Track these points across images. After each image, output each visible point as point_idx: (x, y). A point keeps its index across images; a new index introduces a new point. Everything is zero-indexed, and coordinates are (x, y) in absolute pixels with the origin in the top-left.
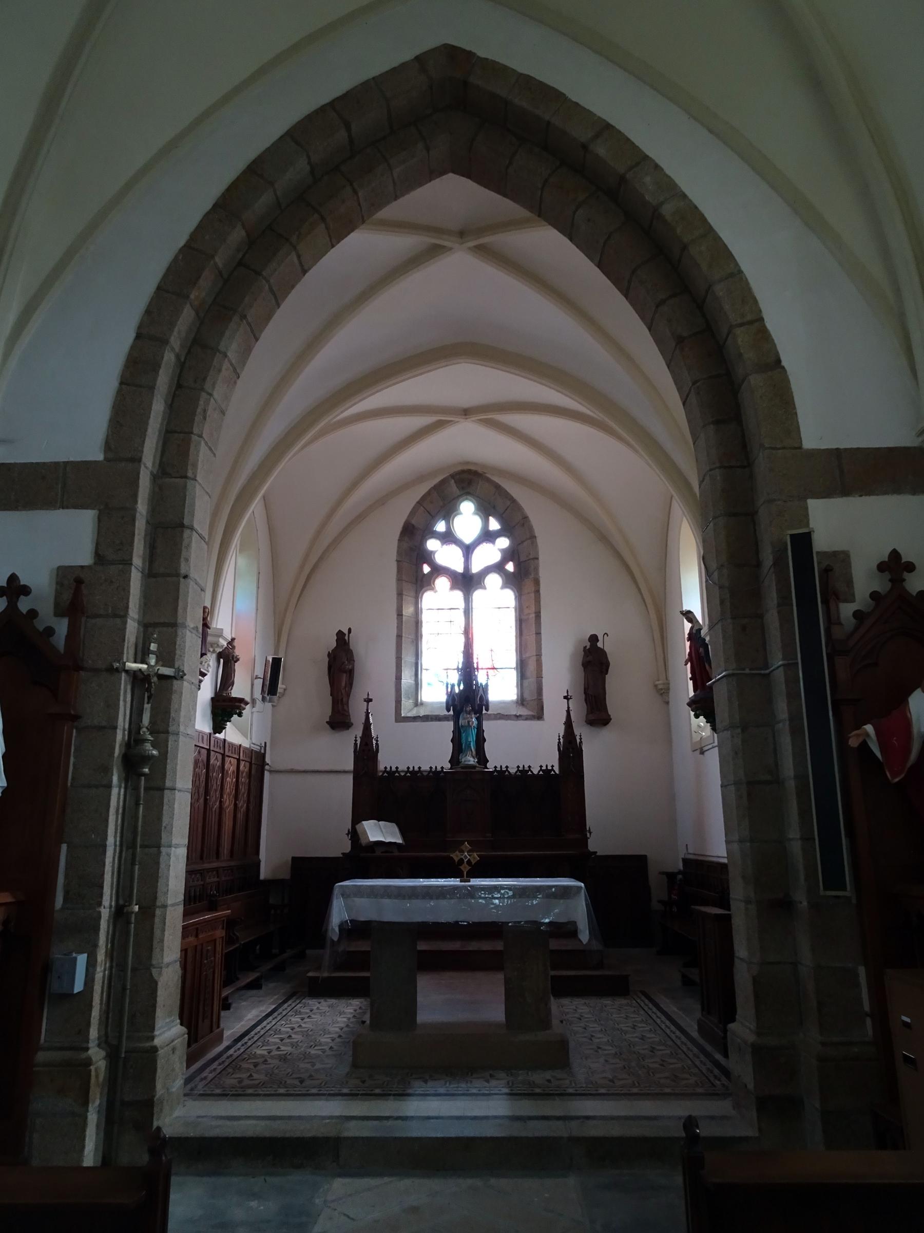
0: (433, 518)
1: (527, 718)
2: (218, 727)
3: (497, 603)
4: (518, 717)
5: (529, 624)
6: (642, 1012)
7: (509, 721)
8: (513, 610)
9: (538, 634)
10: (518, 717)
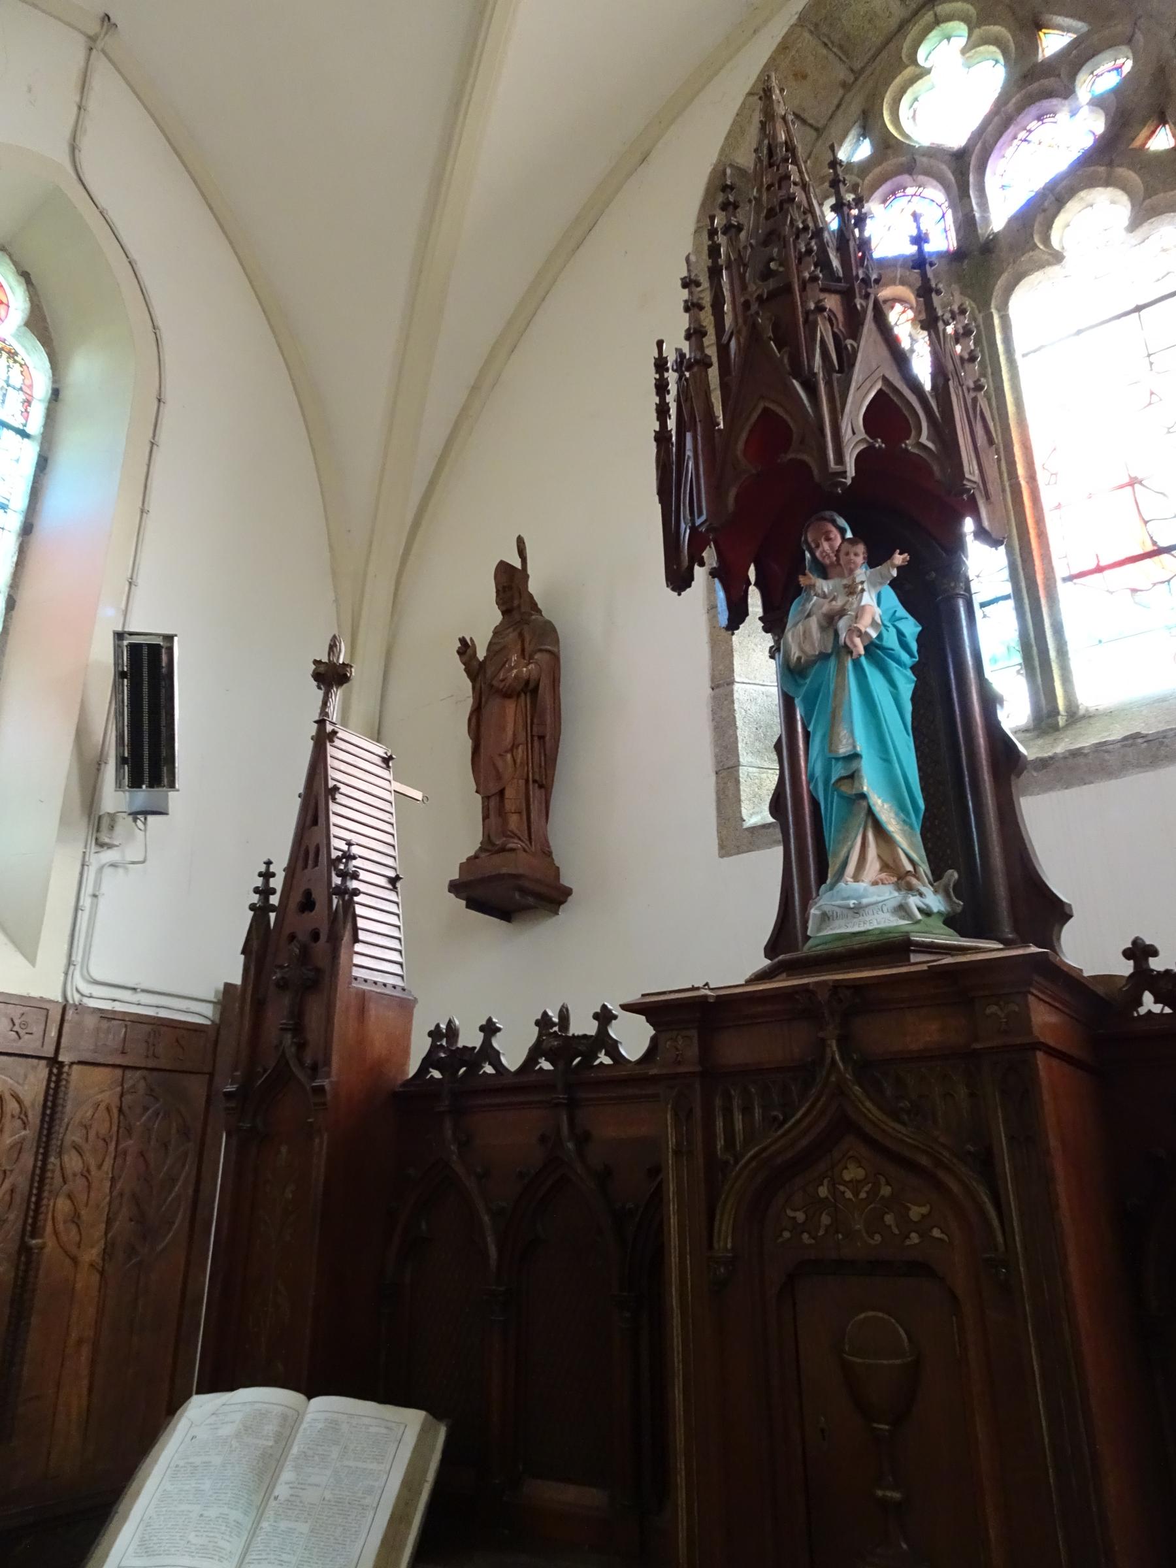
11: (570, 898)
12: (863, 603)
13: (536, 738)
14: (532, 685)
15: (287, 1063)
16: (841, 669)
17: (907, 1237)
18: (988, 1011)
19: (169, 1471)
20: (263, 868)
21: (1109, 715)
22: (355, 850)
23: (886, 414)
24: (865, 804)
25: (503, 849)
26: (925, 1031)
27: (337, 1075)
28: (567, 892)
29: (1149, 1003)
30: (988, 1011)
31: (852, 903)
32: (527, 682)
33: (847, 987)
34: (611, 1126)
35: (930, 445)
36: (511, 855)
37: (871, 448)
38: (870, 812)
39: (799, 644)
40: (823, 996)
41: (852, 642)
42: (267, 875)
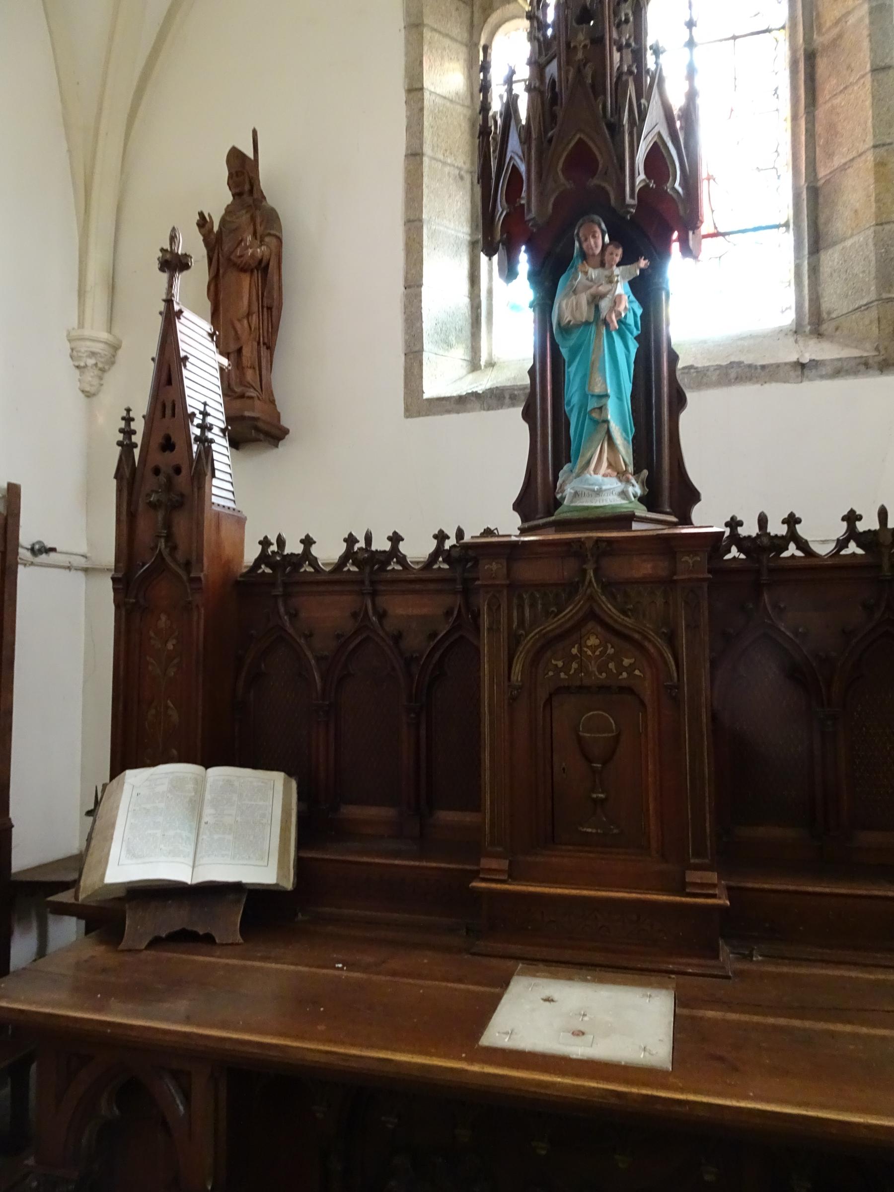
1: (839, 370)
4: (803, 369)
8: (783, 36)
10: (803, 369)
11: (287, 437)
12: (617, 292)
13: (265, 309)
14: (263, 265)
15: (163, 559)
16: (598, 334)
17: (621, 674)
18: (683, 560)
19: (130, 814)
20: (124, 414)
22: (209, 410)
24: (606, 426)
25: (242, 396)
26: (644, 568)
27: (208, 570)
28: (286, 432)
29: (734, 552)
30: (683, 560)
31: (596, 488)
32: (261, 261)
33: (604, 541)
34: (402, 609)
35: (680, 190)
36: (249, 402)
37: (647, 186)
38: (608, 432)
39: (572, 311)
40: (589, 545)
41: (611, 318)
42: (128, 420)
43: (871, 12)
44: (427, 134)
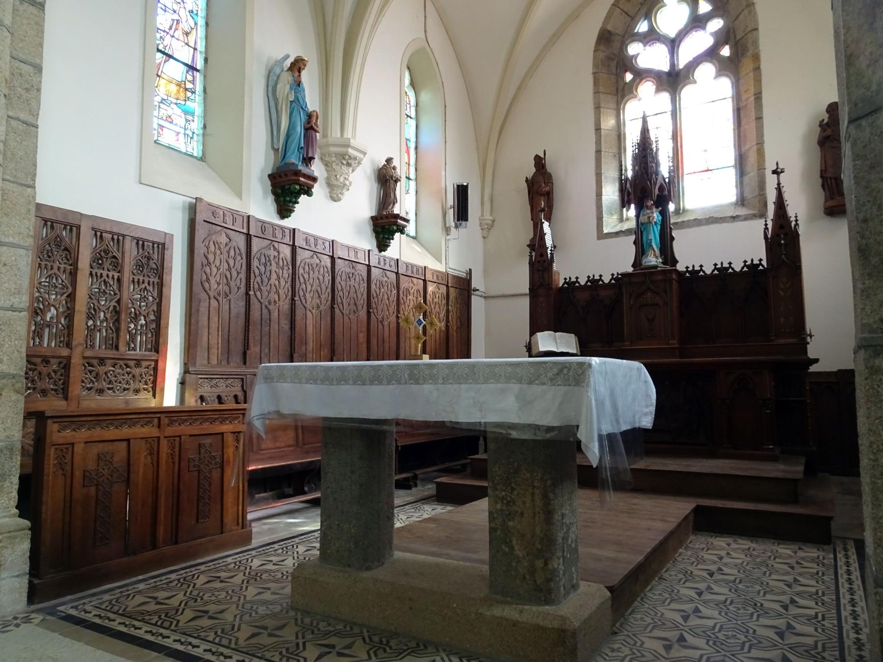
0: (633, 20)
1: (746, 218)
2: (382, 245)
3: (711, 96)
4: (734, 218)
5: (748, 114)
6: (829, 578)
7: (724, 224)
9: (759, 118)
10: (734, 218)
21: (692, 211)
23: (661, 188)
26: (660, 277)
27: (554, 287)
29: (688, 275)
34: (603, 293)
43: (755, 99)
44: (603, 144)
